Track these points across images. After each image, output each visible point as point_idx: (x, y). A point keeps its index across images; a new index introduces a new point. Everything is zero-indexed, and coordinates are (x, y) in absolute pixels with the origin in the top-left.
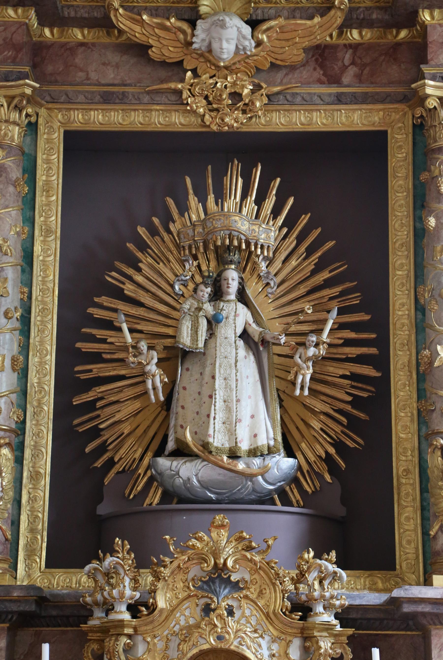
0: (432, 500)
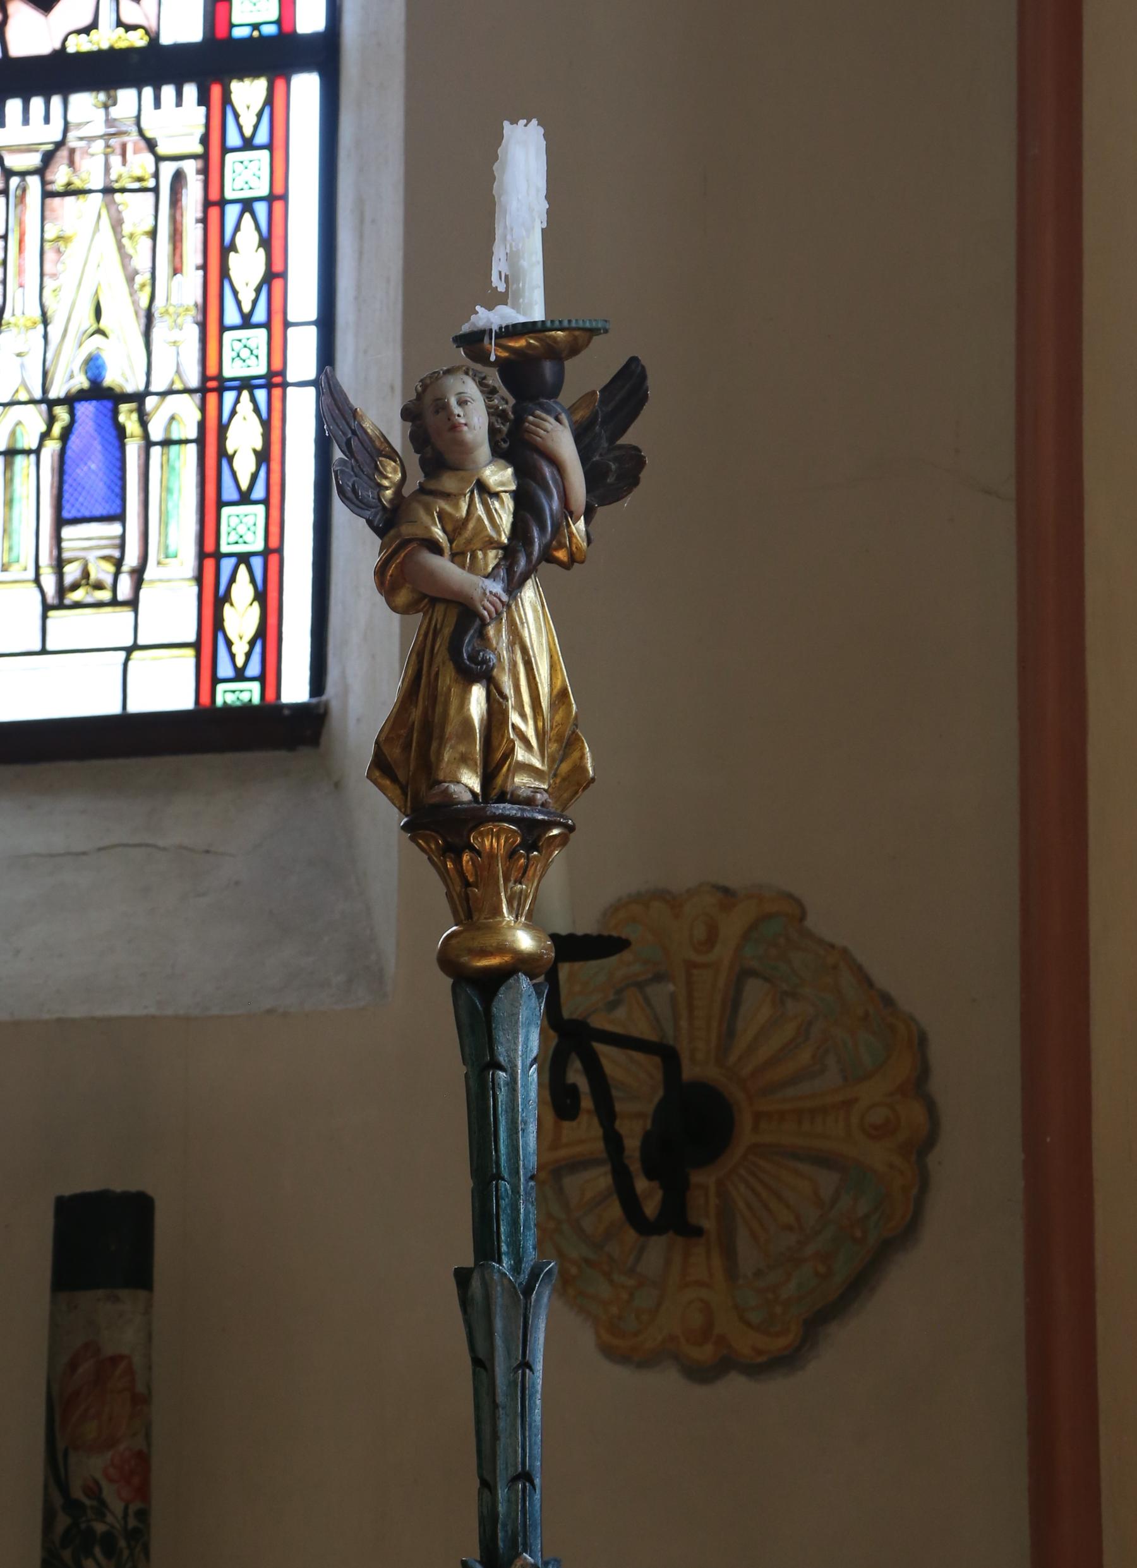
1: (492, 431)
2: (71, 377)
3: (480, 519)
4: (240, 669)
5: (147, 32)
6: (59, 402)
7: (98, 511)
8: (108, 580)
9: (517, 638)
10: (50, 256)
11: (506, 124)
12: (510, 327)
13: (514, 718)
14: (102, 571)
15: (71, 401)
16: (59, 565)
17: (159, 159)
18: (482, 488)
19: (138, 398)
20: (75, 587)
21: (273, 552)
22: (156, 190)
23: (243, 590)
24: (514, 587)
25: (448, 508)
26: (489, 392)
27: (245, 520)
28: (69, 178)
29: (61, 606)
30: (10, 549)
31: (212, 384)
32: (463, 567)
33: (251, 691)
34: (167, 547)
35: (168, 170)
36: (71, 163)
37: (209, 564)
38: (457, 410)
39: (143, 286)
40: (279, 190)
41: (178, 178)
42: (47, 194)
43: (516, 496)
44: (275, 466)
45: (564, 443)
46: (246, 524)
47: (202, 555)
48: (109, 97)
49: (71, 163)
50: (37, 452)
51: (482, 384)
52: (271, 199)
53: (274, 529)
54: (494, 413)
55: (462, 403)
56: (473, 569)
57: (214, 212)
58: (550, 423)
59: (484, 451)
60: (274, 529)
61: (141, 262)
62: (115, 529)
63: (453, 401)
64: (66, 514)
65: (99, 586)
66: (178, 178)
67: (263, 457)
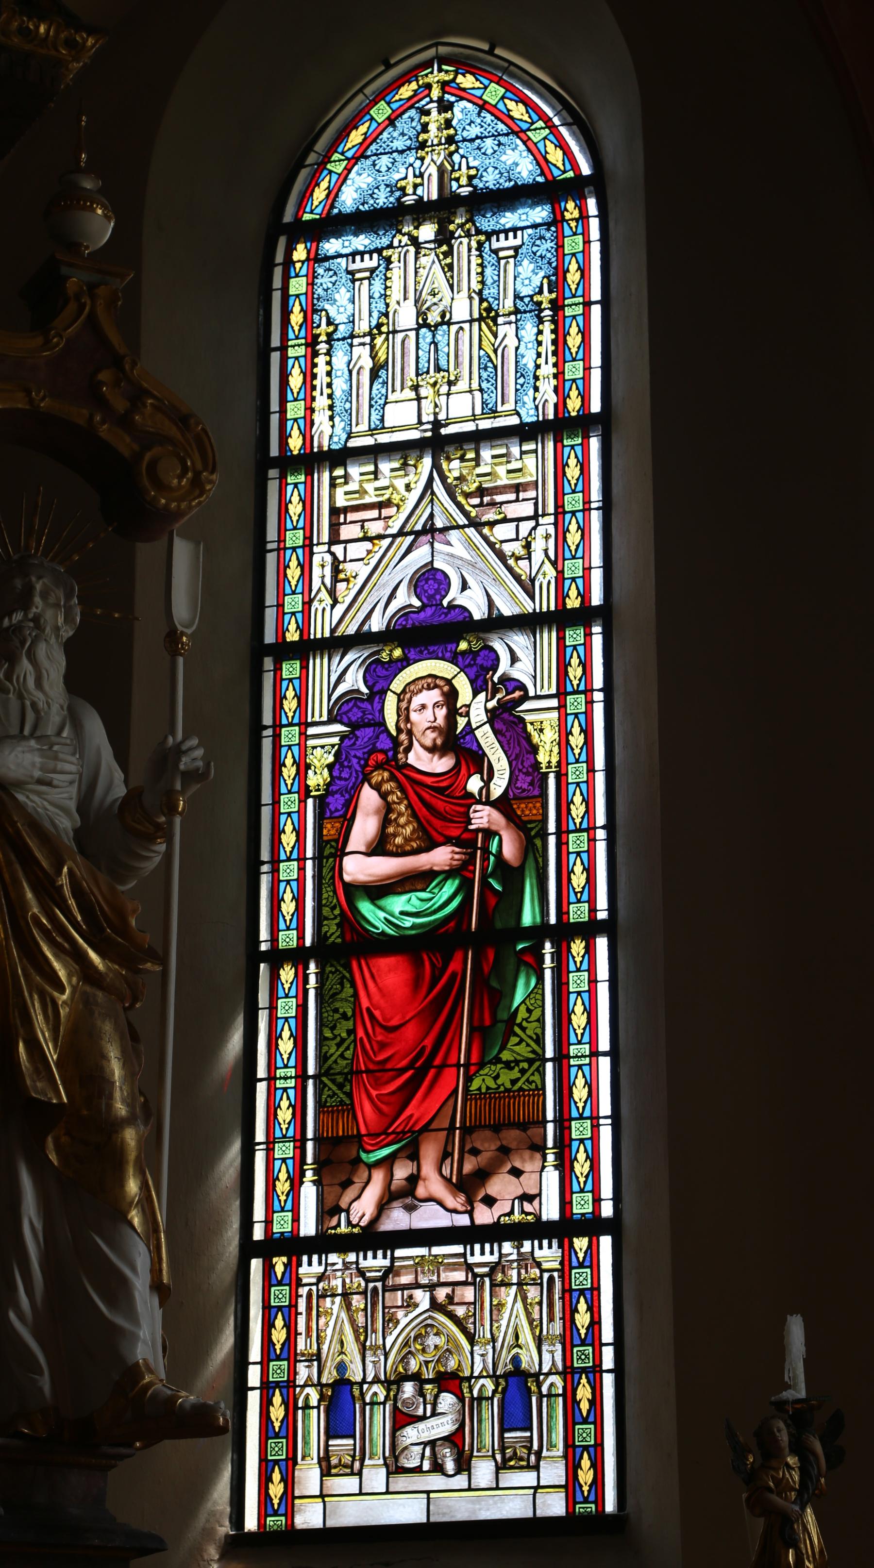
0: (530, 201)
1: (790, 1442)
2: (506, 1365)
3: (788, 1479)
5: (535, 1216)
6: (500, 1376)
7: (520, 1425)
8: (526, 1456)
9: (805, 1529)
10: (495, 1312)
11: (788, 1316)
13: (807, 1563)
14: (522, 1452)
15: (506, 1376)
16: (503, 1449)
17: (542, 1271)
18: (788, 1466)
19: (537, 1375)
20: (511, 1459)
22: (541, 1284)
23: (586, 1463)
24: (803, 1509)
25: (774, 1474)
26: (788, 1426)
29: (505, 1468)
30: (481, 1442)
31: (569, 1370)
32: (781, 1498)
34: (551, 1442)
35: (546, 1276)
36: (503, 1272)
37: (570, 1450)
38: (778, 1434)
39: (537, 1326)
40: (595, 1286)
41: (551, 1280)
42: (493, 1285)
43: (800, 1468)
44: (598, 1407)
45: (818, 1447)
47: (264, 1308)
48: (519, 1243)
49: (503, 1272)
50: (492, 1399)
51: (785, 1422)
52: (592, 1289)
53: (599, 1436)
54: (790, 1435)
55: (779, 1431)
56: (786, 1499)
57: (567, 1295)
58: (812, 1438)
59: (787, 1450)
60: (599, 1436)
61: (536, 1316)
62: (528, 1434)
63: (775, 1430)
64: (505, 1427)
65: (521, 1459)
66: (551, 1280)
67: (592, 1402)
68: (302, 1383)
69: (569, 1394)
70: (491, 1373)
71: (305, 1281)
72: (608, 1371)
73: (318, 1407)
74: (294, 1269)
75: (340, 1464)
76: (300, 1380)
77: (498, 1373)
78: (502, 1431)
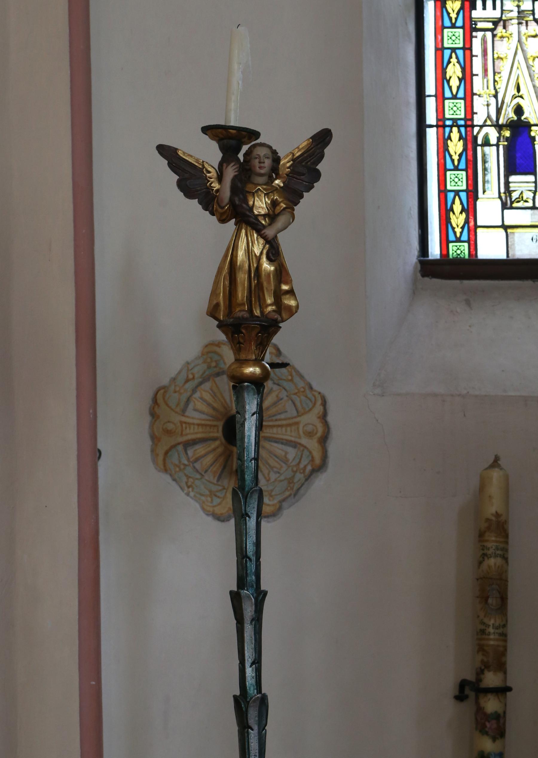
4: (453, 52)
12: (293, 307)
15: (511, 125)
21: (439, 30)
27: (453, 178)
28: (528, 31)
33: (451, 186)
46: (454, 178)
68: (481, 123)
69: (470, 146)
70: (495, 123)
71: (480, 25)
72: (431, 126)
73: (497, 145)
74: (467, 14)
75: (520, 198)
76: (478, 120)
77: (501, 122)
78: (507, 177)
